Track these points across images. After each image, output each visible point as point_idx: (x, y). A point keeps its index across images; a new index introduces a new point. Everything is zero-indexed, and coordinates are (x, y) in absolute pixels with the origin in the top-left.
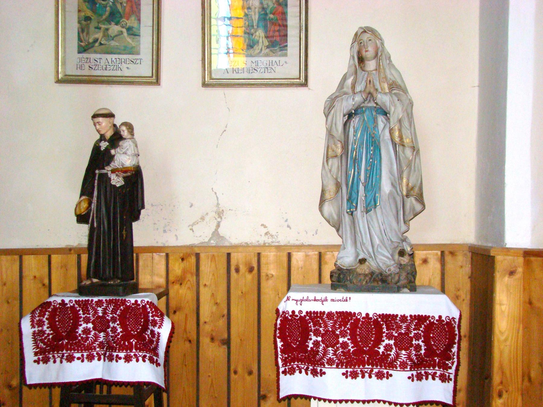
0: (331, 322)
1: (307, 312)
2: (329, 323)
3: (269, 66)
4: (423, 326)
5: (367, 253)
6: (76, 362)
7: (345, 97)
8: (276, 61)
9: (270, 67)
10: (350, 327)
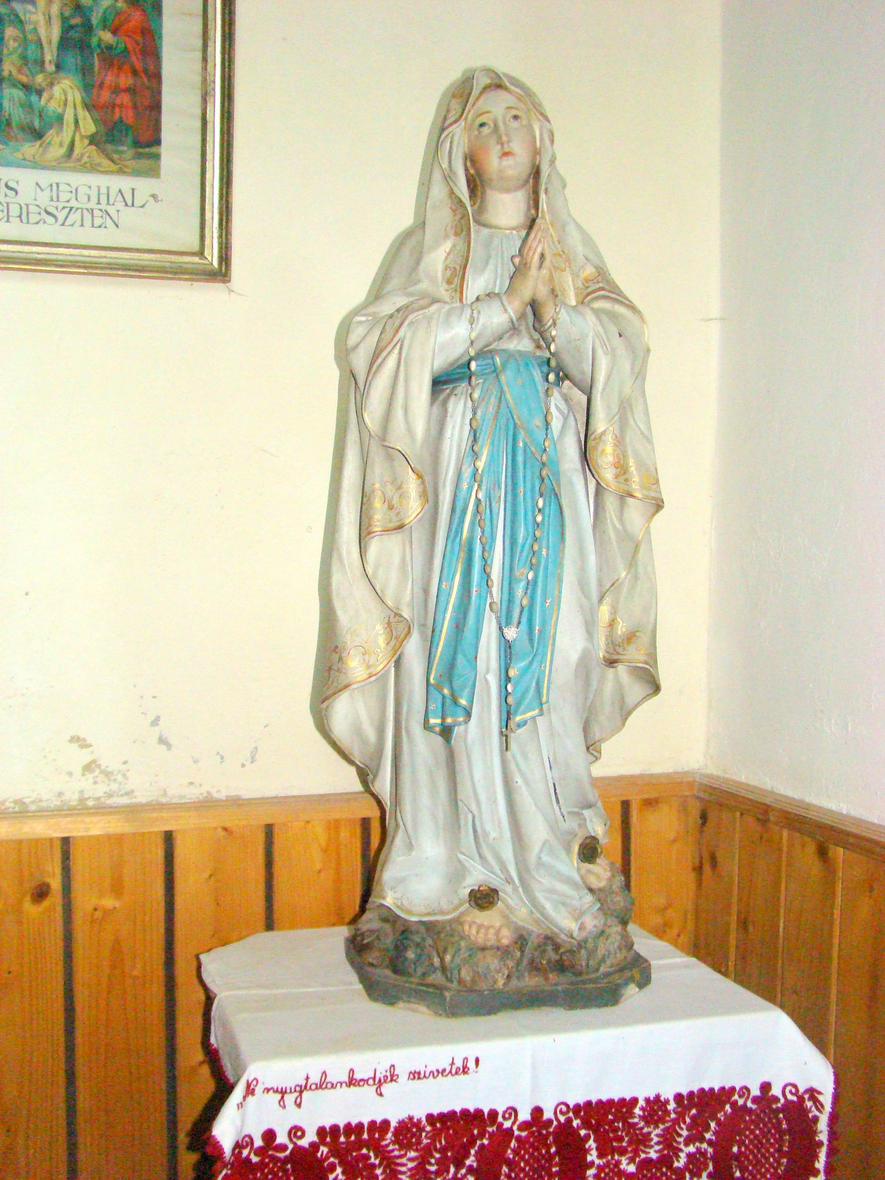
0: (412, 1154)
1: (321, 1131)
2: (404, 1160)
3: (99, 203)
4: (713, 1125)
5: (497, 869)
7: (439, 310)
8: (120, 191)
9: (99, 207)
10: (475, 1165)
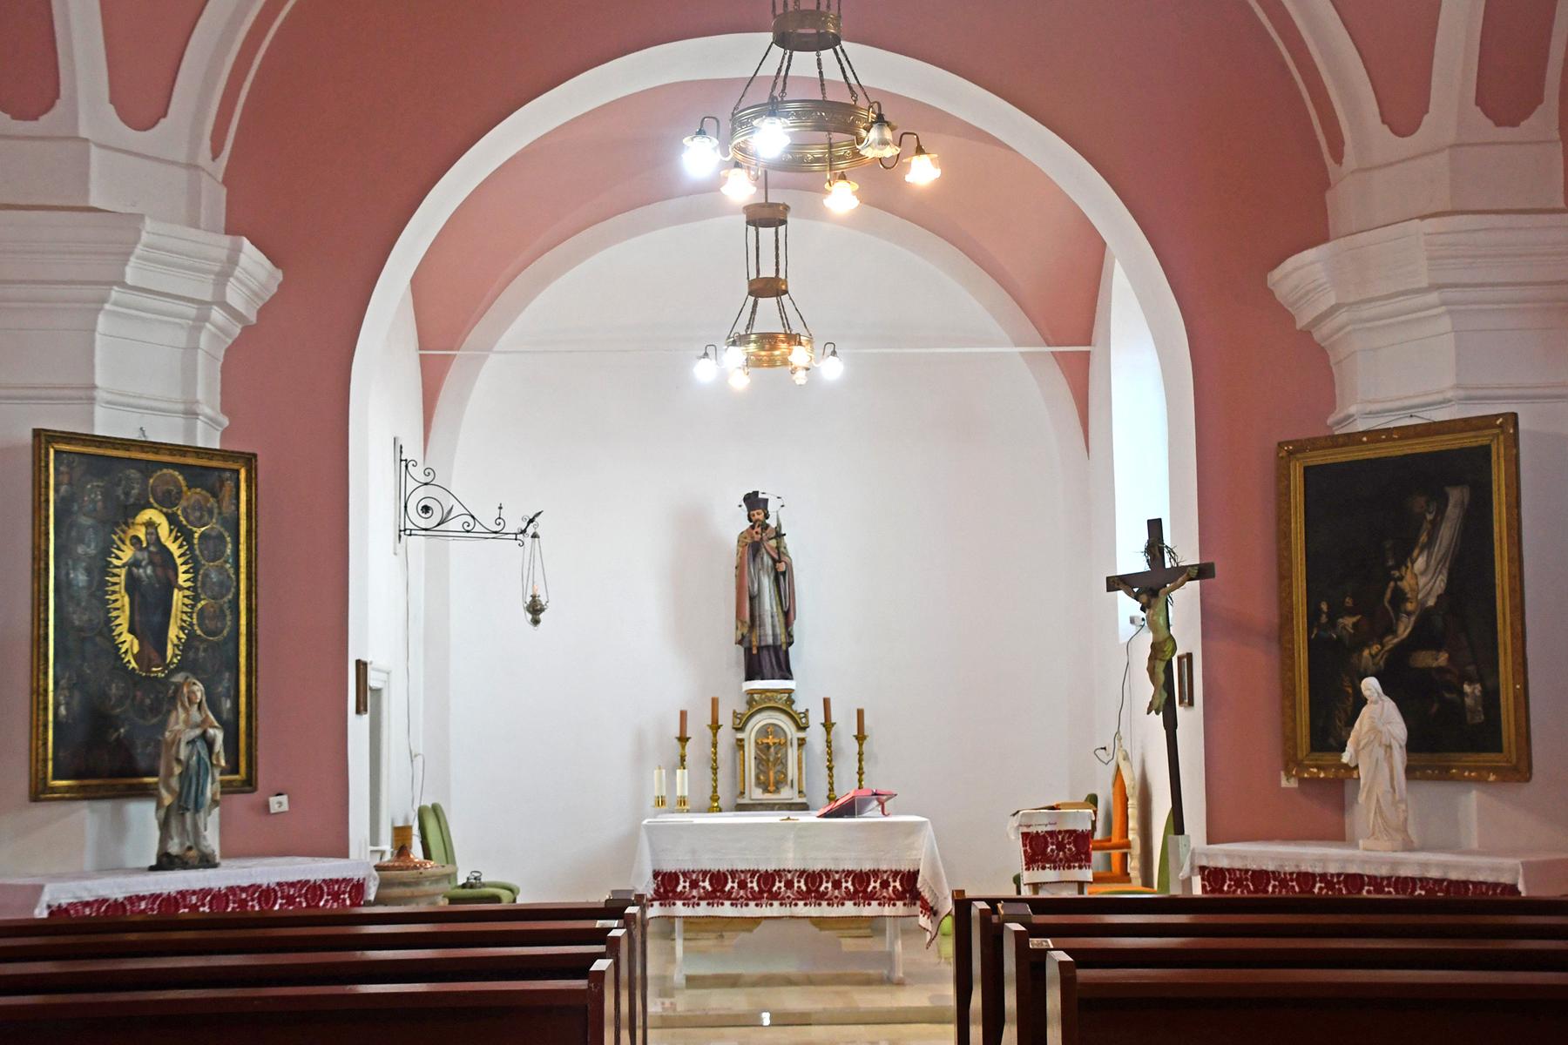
6: (1047, 870)
